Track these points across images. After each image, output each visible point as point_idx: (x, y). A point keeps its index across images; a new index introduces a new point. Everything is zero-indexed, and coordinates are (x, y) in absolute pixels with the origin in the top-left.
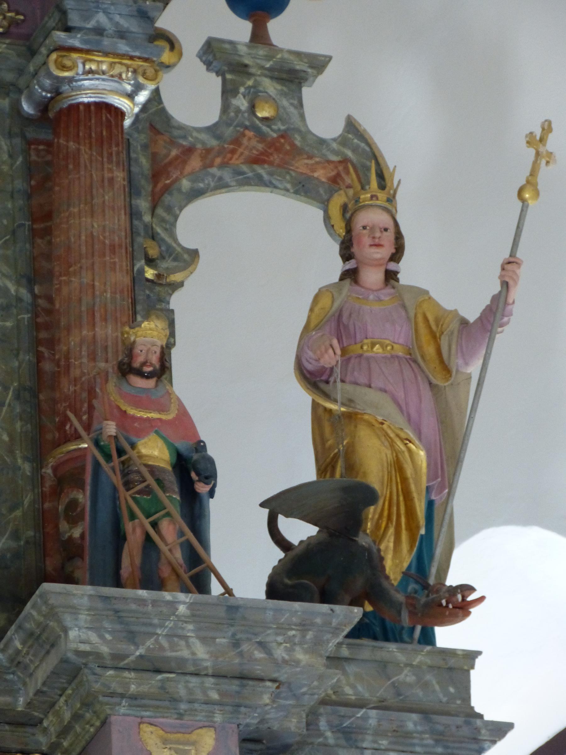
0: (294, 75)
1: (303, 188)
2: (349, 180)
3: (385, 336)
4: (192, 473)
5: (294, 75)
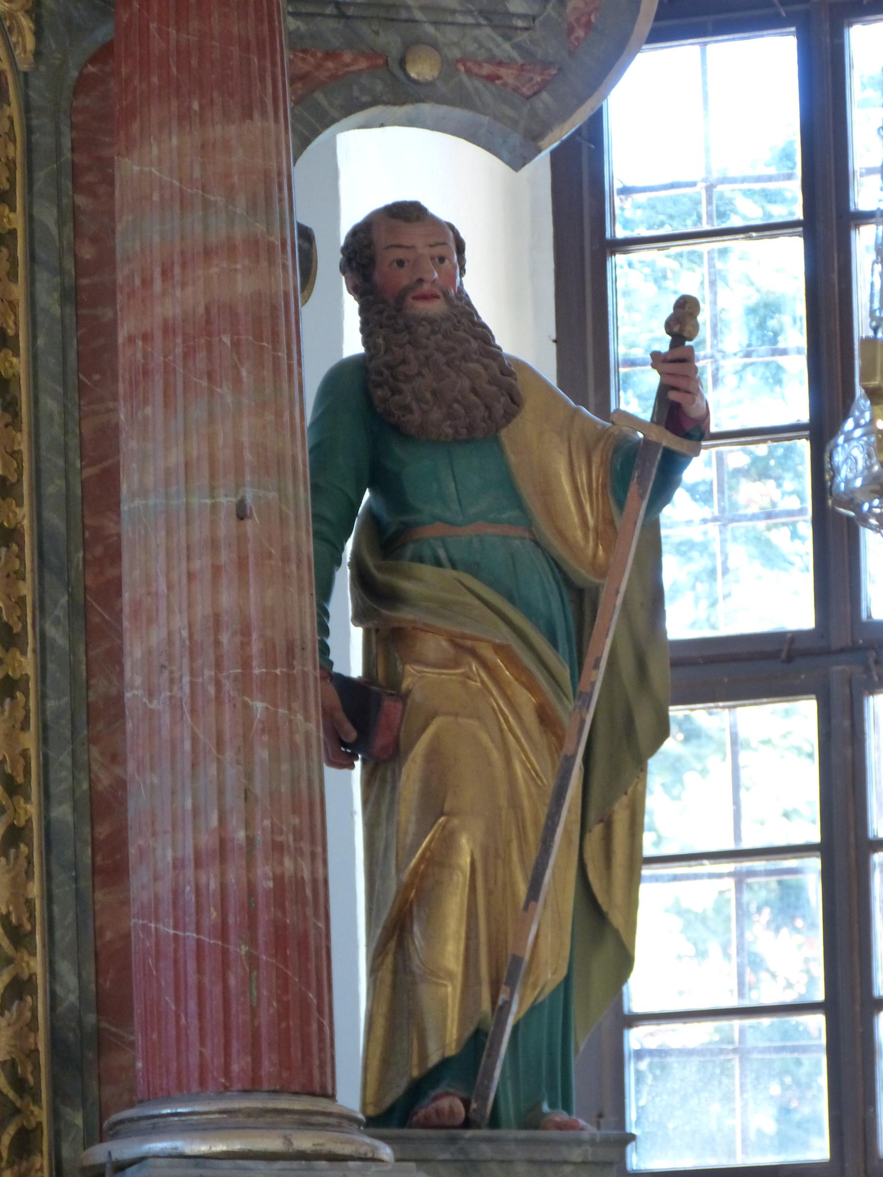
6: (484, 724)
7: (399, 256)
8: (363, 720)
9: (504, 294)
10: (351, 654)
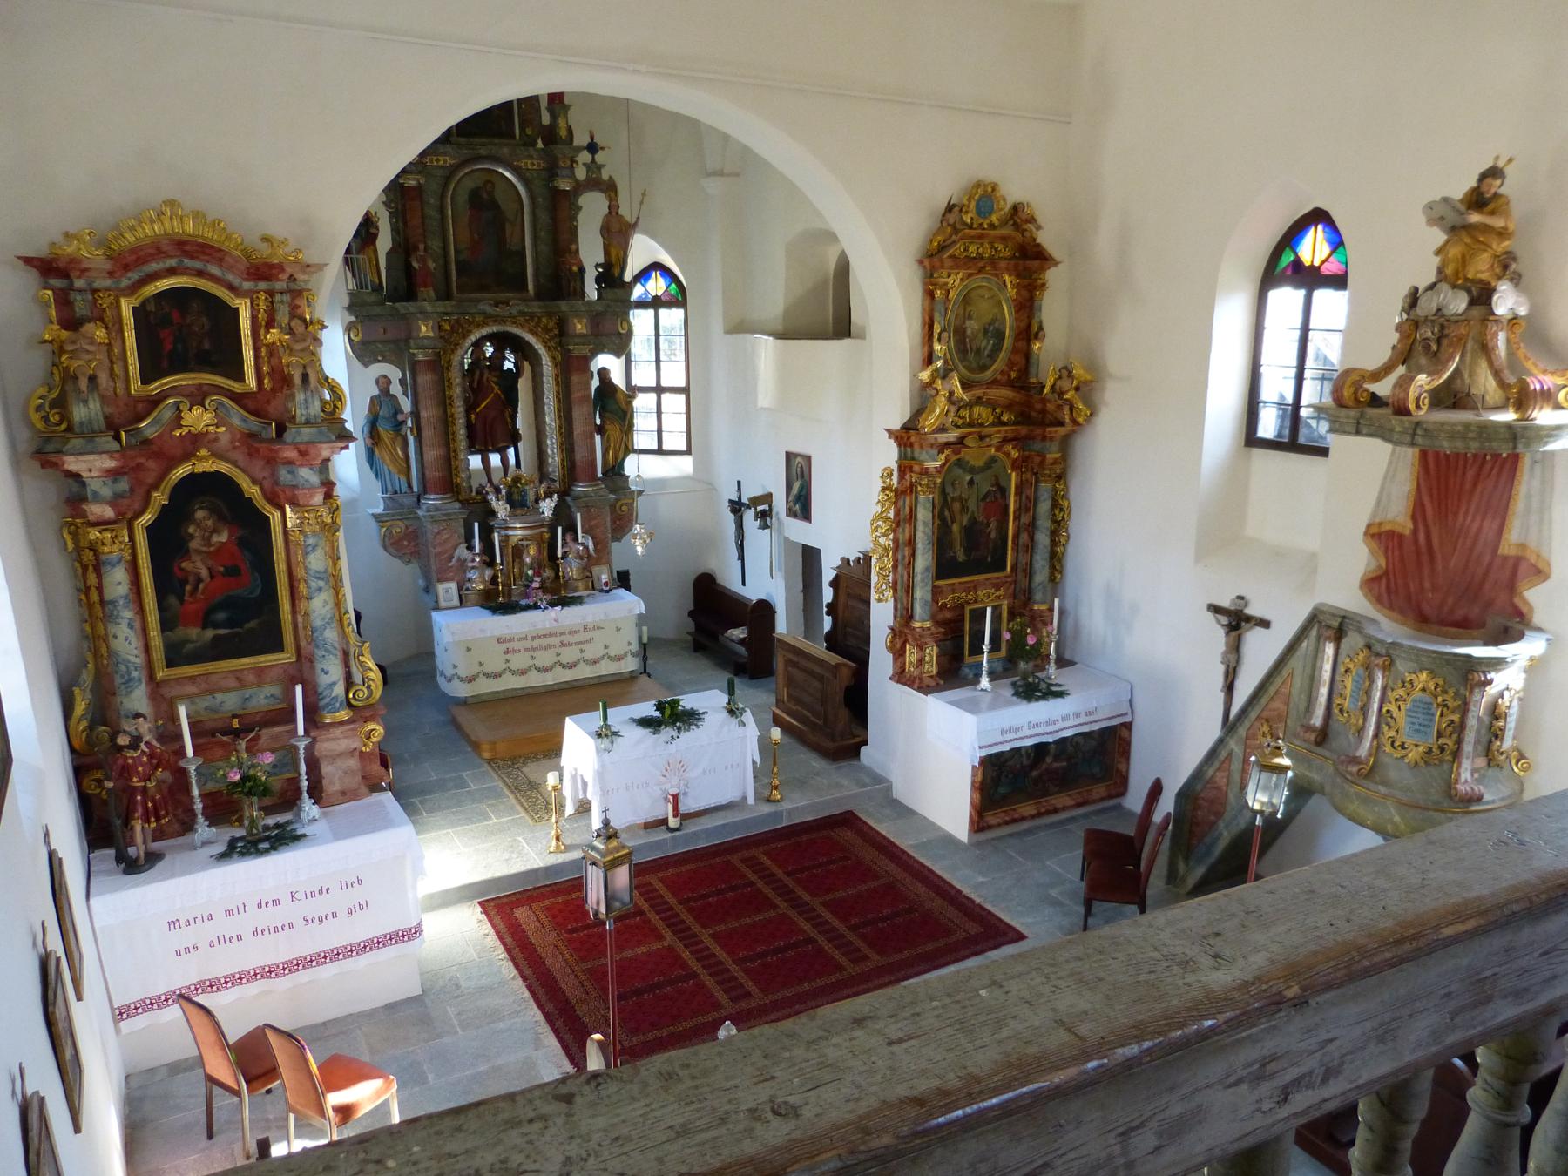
0: (600, 167)
1: (602, 191)
2: (610, 188)
3: (615, 227)
4: (582, 270)
5: (600, 167)
6: (614, 431)
7: (603, 373)
8: (600, 430)
9: (618, 378)
10: (598, 422)
